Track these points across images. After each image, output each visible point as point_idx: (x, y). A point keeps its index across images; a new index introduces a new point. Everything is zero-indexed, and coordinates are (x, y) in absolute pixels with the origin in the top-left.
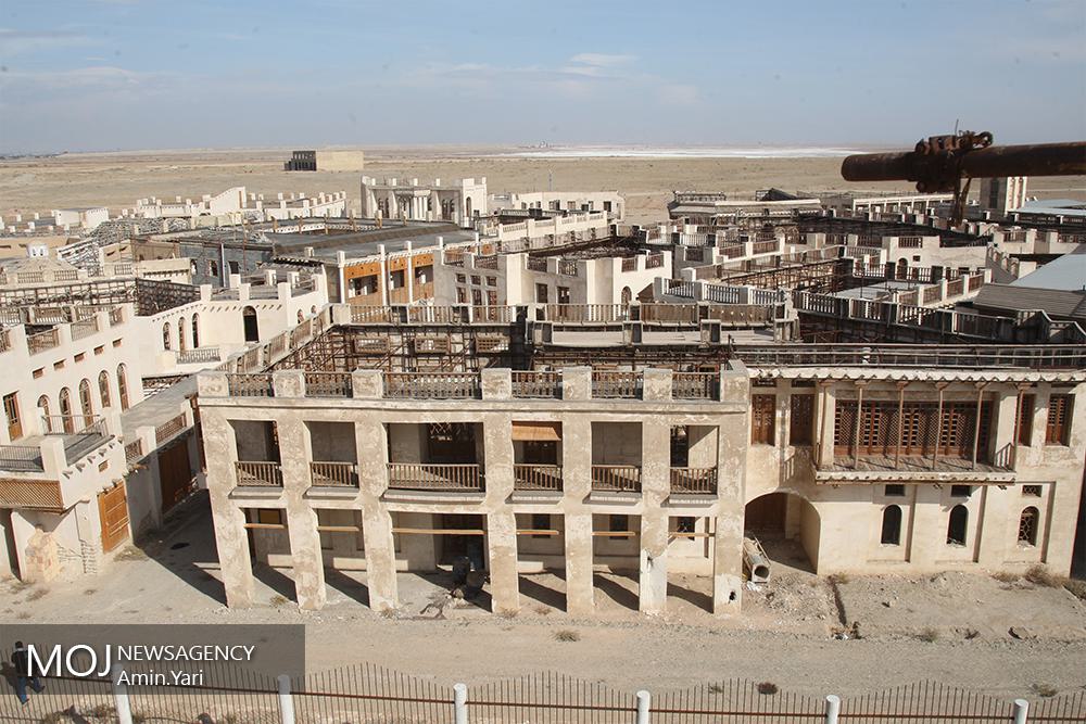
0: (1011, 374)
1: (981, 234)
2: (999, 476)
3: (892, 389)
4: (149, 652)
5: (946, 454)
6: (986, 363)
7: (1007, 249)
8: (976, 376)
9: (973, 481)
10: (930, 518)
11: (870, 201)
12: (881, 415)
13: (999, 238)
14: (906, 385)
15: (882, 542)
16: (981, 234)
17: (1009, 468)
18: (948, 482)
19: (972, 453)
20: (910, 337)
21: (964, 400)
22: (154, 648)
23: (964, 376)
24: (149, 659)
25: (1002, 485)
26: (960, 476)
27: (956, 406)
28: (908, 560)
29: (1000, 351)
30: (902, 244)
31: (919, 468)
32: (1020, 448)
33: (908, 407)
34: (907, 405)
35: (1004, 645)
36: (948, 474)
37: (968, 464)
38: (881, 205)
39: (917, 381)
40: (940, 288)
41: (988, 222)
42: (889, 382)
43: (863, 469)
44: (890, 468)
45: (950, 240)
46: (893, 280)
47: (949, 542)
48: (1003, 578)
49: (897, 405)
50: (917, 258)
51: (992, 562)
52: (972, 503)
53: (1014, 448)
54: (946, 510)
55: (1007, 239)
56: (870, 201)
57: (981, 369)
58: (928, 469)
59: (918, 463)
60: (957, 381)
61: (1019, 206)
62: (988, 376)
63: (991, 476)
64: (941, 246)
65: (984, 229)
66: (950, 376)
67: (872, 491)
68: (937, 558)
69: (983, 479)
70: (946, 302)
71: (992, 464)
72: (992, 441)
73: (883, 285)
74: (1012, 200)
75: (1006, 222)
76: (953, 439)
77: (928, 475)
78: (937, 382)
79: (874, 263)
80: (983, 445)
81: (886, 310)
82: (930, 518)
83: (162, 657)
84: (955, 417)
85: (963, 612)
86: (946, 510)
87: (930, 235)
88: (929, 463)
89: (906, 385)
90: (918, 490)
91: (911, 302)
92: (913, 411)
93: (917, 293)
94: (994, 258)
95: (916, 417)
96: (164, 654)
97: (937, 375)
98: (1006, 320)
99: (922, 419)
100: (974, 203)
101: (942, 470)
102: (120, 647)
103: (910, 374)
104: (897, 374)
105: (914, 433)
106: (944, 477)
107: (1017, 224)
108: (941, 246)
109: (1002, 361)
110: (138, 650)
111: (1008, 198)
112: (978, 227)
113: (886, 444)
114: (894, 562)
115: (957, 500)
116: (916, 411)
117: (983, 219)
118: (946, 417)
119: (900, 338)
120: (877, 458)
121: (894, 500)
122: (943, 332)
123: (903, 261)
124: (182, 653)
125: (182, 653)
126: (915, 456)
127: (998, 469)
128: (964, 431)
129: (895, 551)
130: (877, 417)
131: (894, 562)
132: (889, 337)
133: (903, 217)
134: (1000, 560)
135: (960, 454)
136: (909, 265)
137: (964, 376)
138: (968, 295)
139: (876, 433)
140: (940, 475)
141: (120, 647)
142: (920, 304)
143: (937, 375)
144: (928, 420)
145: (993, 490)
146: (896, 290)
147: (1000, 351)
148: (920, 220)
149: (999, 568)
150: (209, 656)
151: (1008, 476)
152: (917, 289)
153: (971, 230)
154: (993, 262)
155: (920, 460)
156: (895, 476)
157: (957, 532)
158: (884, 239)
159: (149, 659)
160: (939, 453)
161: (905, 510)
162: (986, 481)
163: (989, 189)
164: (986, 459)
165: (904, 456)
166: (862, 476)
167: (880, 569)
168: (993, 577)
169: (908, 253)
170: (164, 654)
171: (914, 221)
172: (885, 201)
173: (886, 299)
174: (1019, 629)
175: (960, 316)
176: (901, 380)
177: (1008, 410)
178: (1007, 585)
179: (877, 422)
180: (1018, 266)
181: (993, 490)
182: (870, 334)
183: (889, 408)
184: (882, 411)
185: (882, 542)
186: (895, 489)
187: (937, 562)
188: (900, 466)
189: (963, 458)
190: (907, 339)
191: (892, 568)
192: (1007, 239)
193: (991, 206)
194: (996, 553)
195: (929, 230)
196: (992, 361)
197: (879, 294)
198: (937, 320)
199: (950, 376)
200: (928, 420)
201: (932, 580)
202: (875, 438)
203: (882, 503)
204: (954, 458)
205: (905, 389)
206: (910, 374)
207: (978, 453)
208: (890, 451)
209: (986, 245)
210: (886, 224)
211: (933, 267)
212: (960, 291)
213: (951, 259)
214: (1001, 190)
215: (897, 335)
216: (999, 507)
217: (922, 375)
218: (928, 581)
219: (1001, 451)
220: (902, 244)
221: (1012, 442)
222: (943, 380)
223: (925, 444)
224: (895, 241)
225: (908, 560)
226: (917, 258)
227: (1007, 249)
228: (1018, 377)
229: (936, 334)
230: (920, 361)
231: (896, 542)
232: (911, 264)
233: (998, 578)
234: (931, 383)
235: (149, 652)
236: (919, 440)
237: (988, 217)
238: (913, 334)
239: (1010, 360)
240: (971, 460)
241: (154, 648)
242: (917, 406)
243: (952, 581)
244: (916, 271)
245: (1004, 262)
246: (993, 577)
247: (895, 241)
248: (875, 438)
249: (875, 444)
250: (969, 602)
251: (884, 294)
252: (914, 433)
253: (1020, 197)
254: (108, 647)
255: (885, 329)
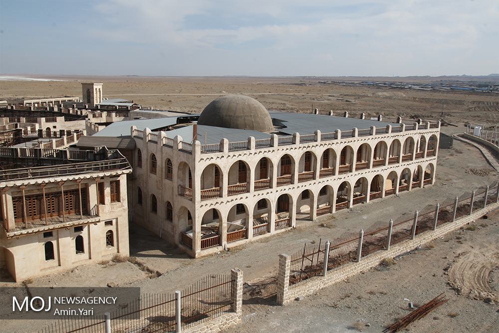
0: (92, 175)
1: (83, 115)
2: (93, 220)
3: (39, 188)
4: (69, 300)
5: (69, 214)
6: (81, 171)
7: (94, 121)
8: (77, 177)
9: (83, 224)
10: (67, 244)
11: (32, 101)
12: (36, 201)
13: (90, 116)
14: (45, 185)
15: (46, 260)
16: (83, 115)
17: (97, 215)
18: (71, 226)
19: (80, 212)
20: (50, 163)
21: (73, 188)
22: (71, 298)
23: (71, 178)
24: (69, 303)
25: (95, 223)
26: (76, 222)
27: (70, 192)
28: (60, 265)
29: (86, 165)
30: (47, 121)
31: (57, 223)
32: (101, 206)
33: (48, 195)
34: (47, 195)
35: (105, 292)
36: (71, 223)
37: (79, 217)
38: (38, 103)
39: (50, 183)
40: (63, 140)
41: (87, 109)
42: (37, 185)
43: (31, 228)
44: (44, 225)
45: (69, 118)
46: (42, 137)
47: (77, 253)
48: (103, 263)
49: (43, 195)
50: (55, 127)
51: (97, 257)
52: (84, 234)
53: (98, 206)
54: (73, 239)
55: (94, 116)
56: (32, 101)
57: (78, 174)
58: (61, 222)
59: (57, 220)
60: (68, 181)
61: (100, 102)
62: (82, 176)
63: (90, 220)
64: (65, 121)
65: (84, 112)
66: (65, 178)
67: (37, 237)
68: (73, 261)
69: (86, 222)
70: (66, 146)
71: (90, 215)
72: (88, 204)
73: (37, 140)
74: (97, 100)
75: (94, 109)
76: (71, 207)
77: (61, 225)
78: (59, 182)
79: (33, 130)
80: (84, 207)
81: (37, 152)
82: (67, 244)
83: (74, 302)
84: (71, 197)
85: (87, 282)
86: (73, 239)
87: (59, 116)
88: (61, 219)
89: (45, 185)
90: (59, 232)
91: (50, 147)
92: (51, 197)
93: (52, 143)
94: (89, 125)
95: (53, 199)
96: (75, 301)
97: (59, 179)
98: (90, 152)
99: (55, 200)
100: (81, 101)
101: (68, 222)
102: (55, 298)
103: (46, 180)
104: (40, 181)
105: (53, 207)
106: (69, 224)
107: (99, 110)
108: (65, 121)
109: (88, 169)
110: (64, 299)
111: (95, 99)
112: (82, 112)
113: (40, 214)
114: (53, 267)
115: (77, 234)
116: (52, 197)
117: (85, 108)
118: (67, 197)
119: (44, 164)
120: (37, 221)
121: (49, 239)
122: (64, 159)
123: (48, 129)
124: (84, 300)
125: (84, 300)
126: (55, 217)
127: (92, 217)
128: (76, 203)
129: (53, 263)
130: (34, 202)
131: (53, 267)
132: (39, 164)
133: (48, 108)
134: (100, 255)
135: (75, 213)
136: (51, 130)
137: (71, 178)
138: (76, 142)
139: (35, 209)
140: (67, 224)
141: (55, 298)
142: (54, 147)
143: (59, 179)
144: (59, 200)
145: (92, 226)
146: (41, 142)
147: (86, 165)
148: (56, 109)
149: (100, 259)
150: (96, 302)
151: (97, 219)
152: (52, 141)
153: (79, 113)
154: (89, 128)
155: (57, 219)
156: (46, 228)
157: (80, 247)
158: (38, 119)
159: (69, 303)
160: (65, 214)
161: (54, 243)
162: (88, 223)
163: (86, 95)
164: (87, 213)
165: (50, 218)
166: (30, 231)
167: (47, 272)
168: (99, 264)
169: (50, 125)
170: (75, 301)
171: (53, 110)
172: (40, 101)
173: (37, 147)
174: (111, 283)
175: (70, 152)
176: (42, 183)
177: (93, 190)
178: (105, 266)
179: (34, 204)
180: (98, 127)
181: (92, 226)
182: (30, 164)
183: (39, 197)
184: (36, 199)
185: (46, 260)
186: (48, 234)
187: (73, 263)
188: (48, 223)
189: (77, 215)
190: (49, 164)
191: (53, 270)
192: (94, 116)
193: (88, 103)
194: (98, 253)
195: (60, 114)
196: (83, 170)
197: (33, 145)
198: (62, 153)
199: (65, 178)
200: (59, 200)
201: (72, 272)
202: (35, 212)
203: (42, 242)
204: (73, 215)
205: (45, 187)
206: (46, 180)
207: (82, 212)
208: (43, 217)
209: (84, 119)
210: (40, 112)
211: (60, 131)
212: (73, 140)
213: (71, 126)
214: (91, 95)
215: (43, 163)
216: (96, 233)
217: (52, 180)
218: (70, 272)
219: (93, 208)
220: (47, 121)
221: (97, 204)
222: (62, 181)
223: (59, 211)
224: (43, 119)
225: (60, 265)
226: (55, 127)
227: (94, 121)
228: (95, 175)
229: (61, 161)
230: (51, 174)
231: (113, 245)
232: (52, 130)
233: (101, 264)
234: (56, 183)
235: (69, 300)
236: (56, 209)
237: (87, 107)
238: (50, 162)
239: (91, 169)
240: (80, 214)
241: (71, 298)
242: (52, 194)
243: (81, 270)
244: (55, 133)
245: (93, 127)
246: (99, 264)
247: (43, 119)
248: (35, 212)
249: (35, 215)
250: (89, 277)
251: (36, 144)
252: (53, 207)
253: (100, 98)
254: (50, 298)
255: (37, 160)
